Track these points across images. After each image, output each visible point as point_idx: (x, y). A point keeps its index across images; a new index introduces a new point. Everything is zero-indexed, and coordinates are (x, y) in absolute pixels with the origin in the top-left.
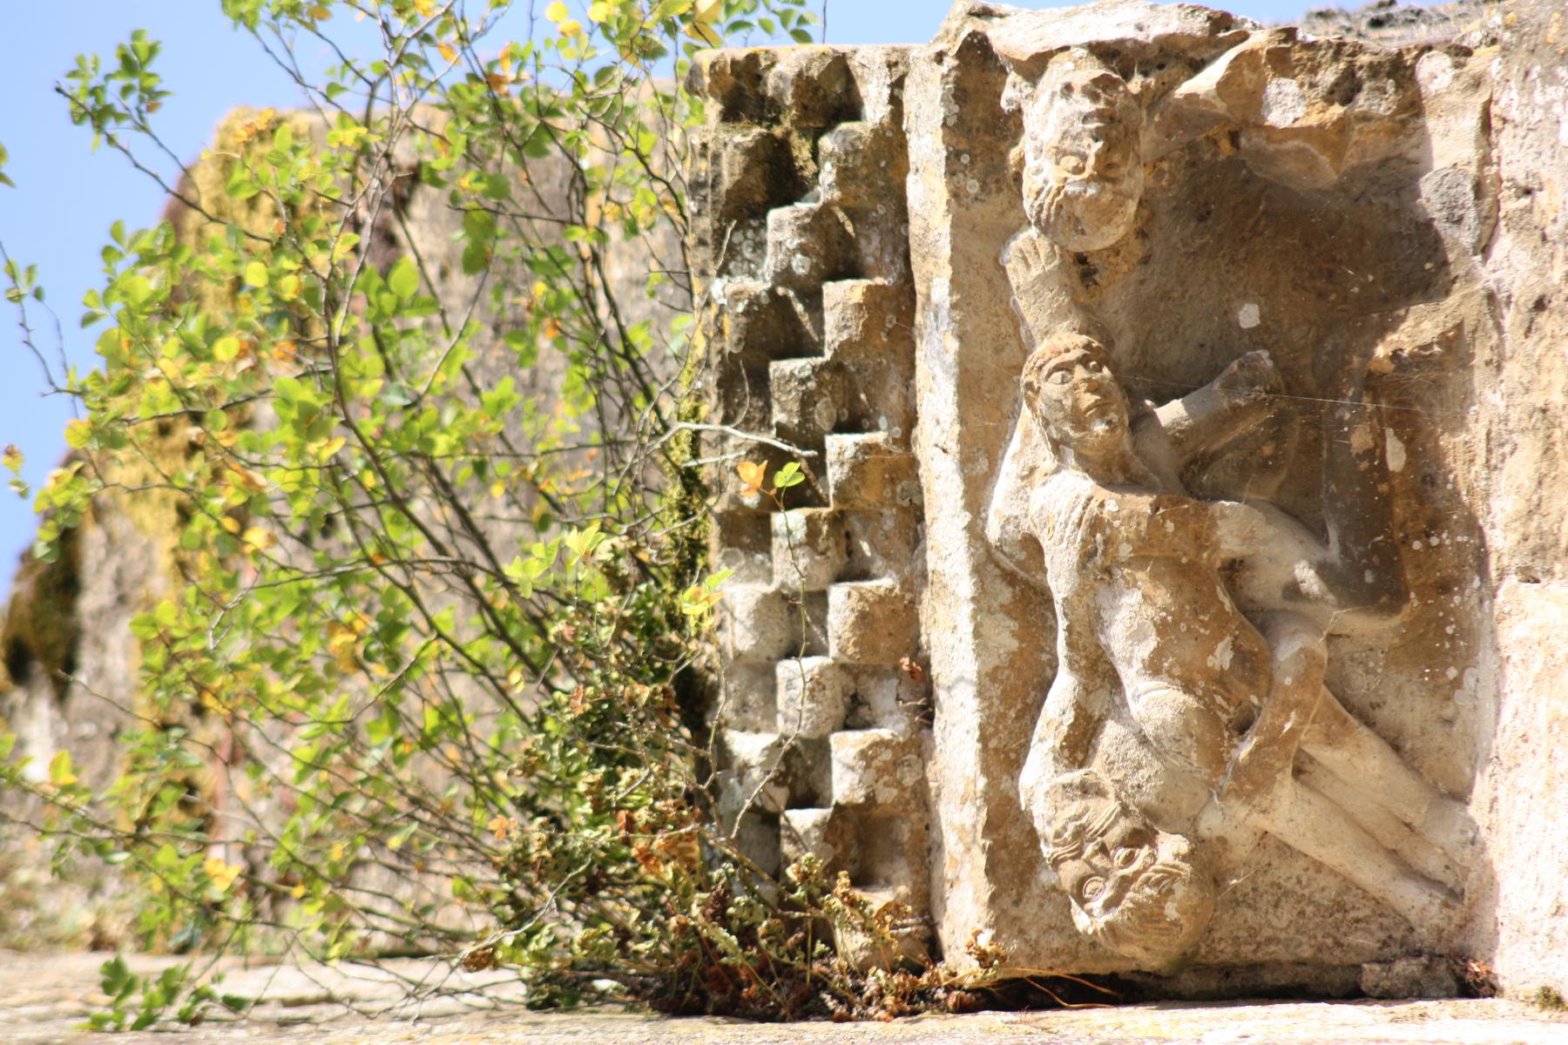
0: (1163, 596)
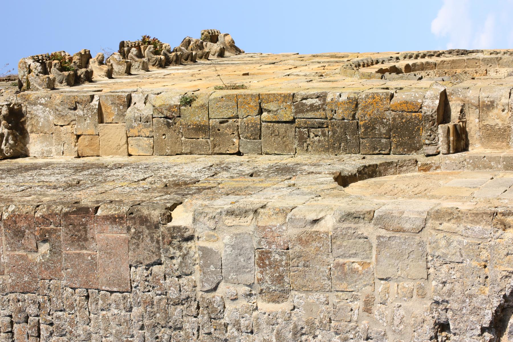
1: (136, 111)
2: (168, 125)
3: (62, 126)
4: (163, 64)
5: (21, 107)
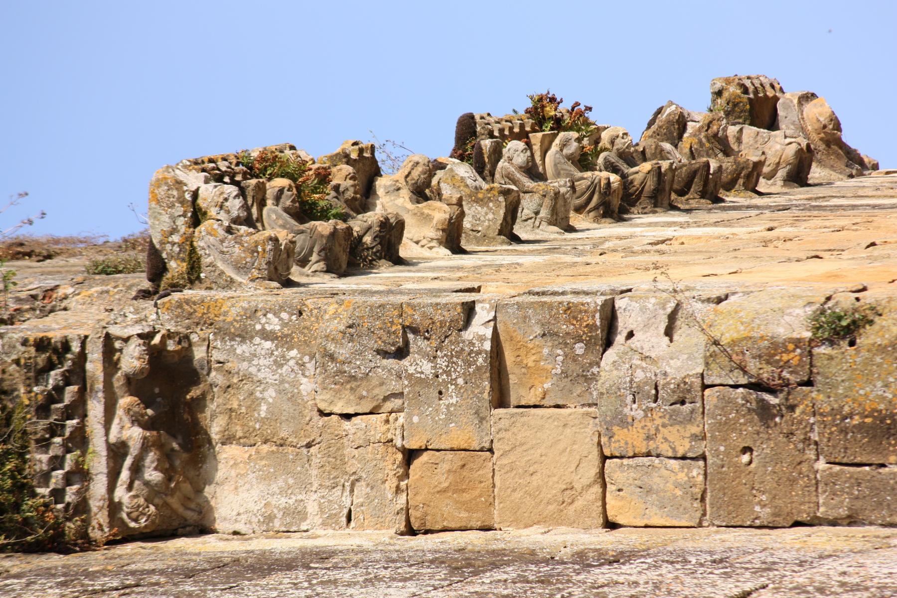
0: (158, 453)
1: (636, 362)
2: (765, 413)
3: (347, 417)
4: (616, 202)
5: (190, 345)
